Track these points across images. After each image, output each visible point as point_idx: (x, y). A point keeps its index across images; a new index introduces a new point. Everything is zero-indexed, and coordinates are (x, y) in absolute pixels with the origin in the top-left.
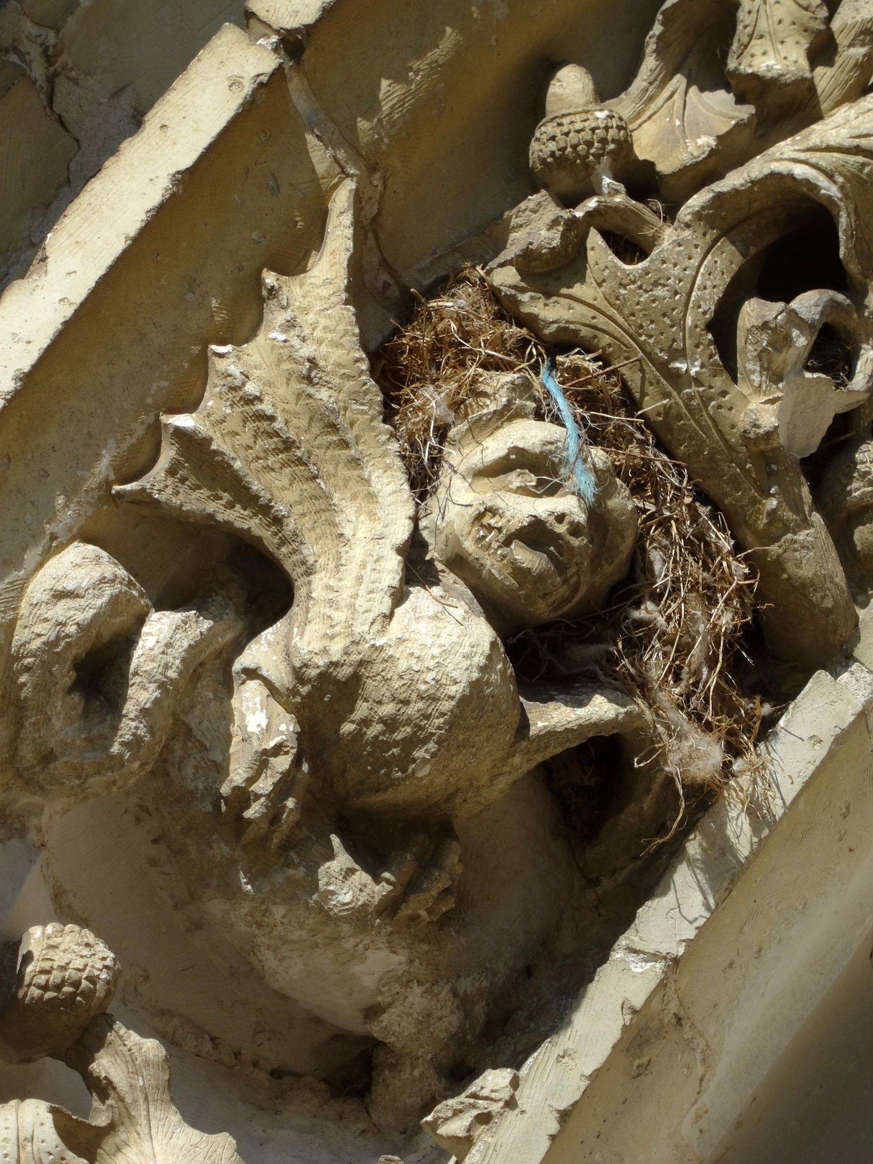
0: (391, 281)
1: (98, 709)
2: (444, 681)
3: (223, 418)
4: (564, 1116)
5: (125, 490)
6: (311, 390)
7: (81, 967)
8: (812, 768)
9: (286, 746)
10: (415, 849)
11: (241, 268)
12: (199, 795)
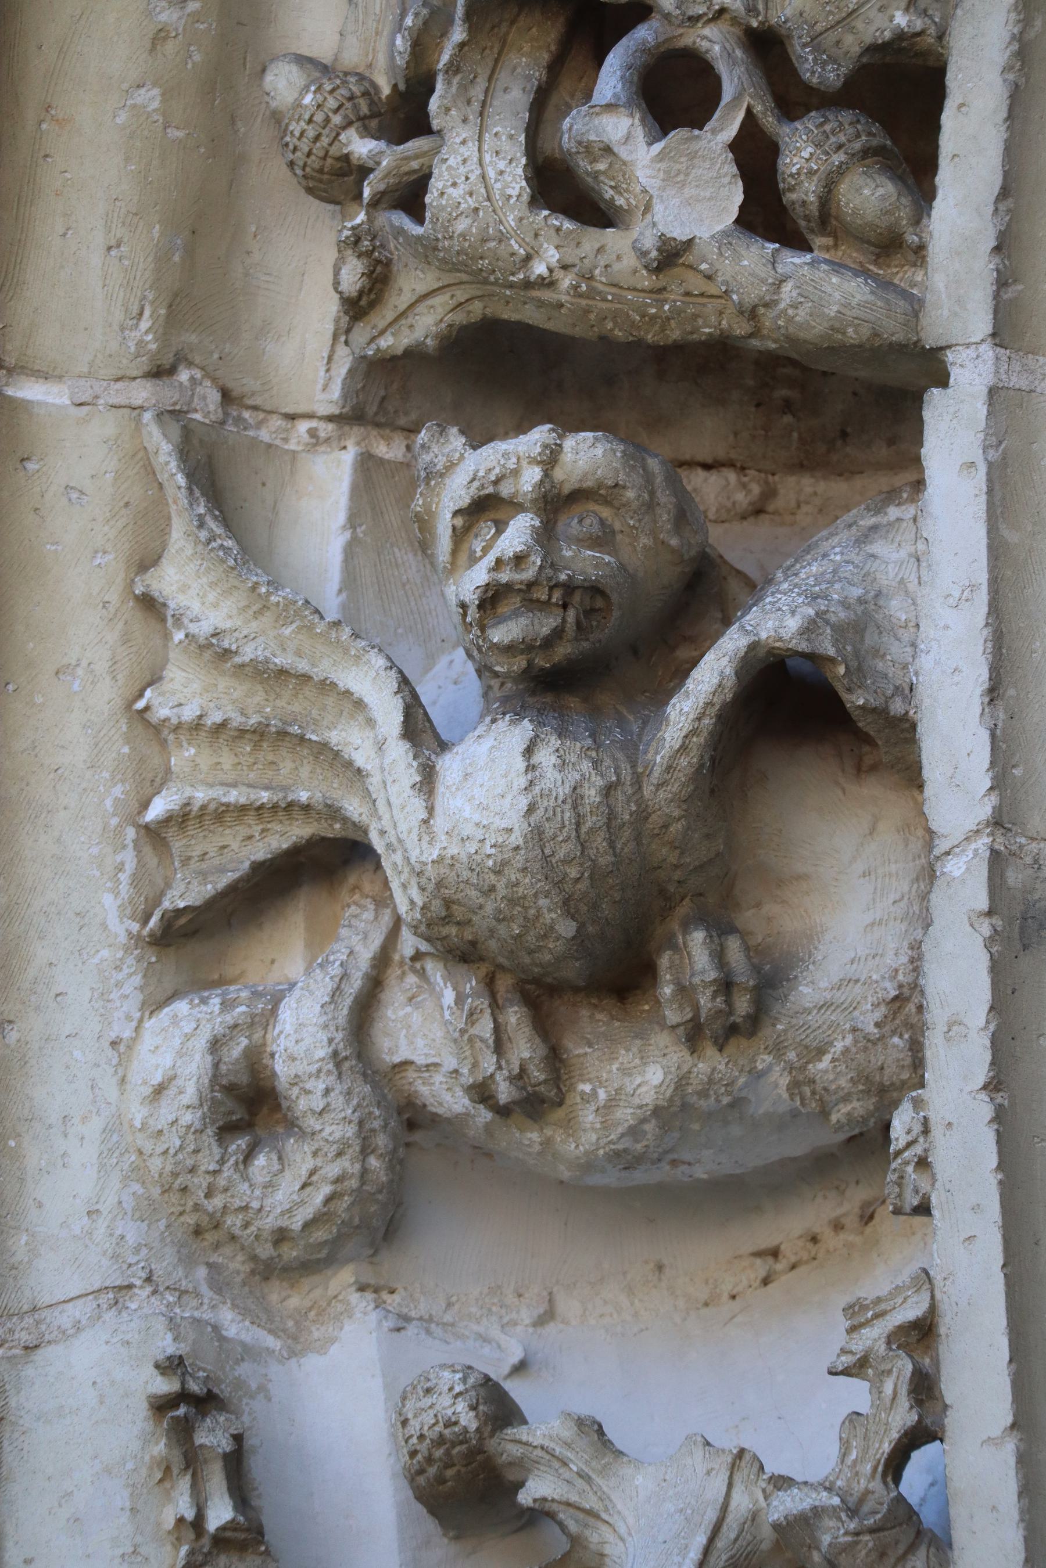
0: (313, 424)
1: (296, 1146)
2: (500, 840)
3: (192, 764)
4: (992, 1086)
5: (151, 930)
6: (238, 660)
7: (433, 1421)
8: (983, 498)
9: (476, 1008)
10: (668, 977)
11: (105, 604)
12: (473, 1112)
